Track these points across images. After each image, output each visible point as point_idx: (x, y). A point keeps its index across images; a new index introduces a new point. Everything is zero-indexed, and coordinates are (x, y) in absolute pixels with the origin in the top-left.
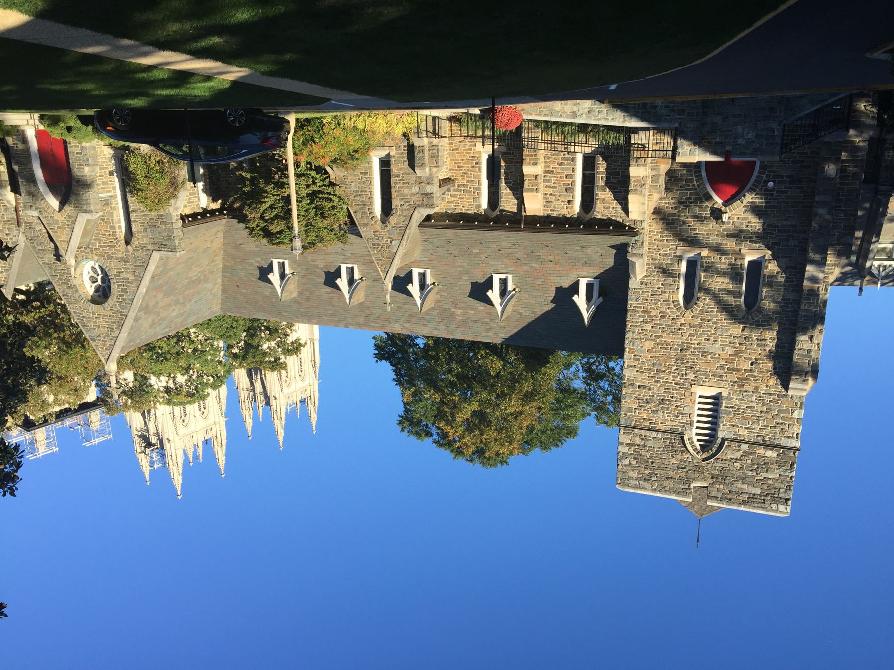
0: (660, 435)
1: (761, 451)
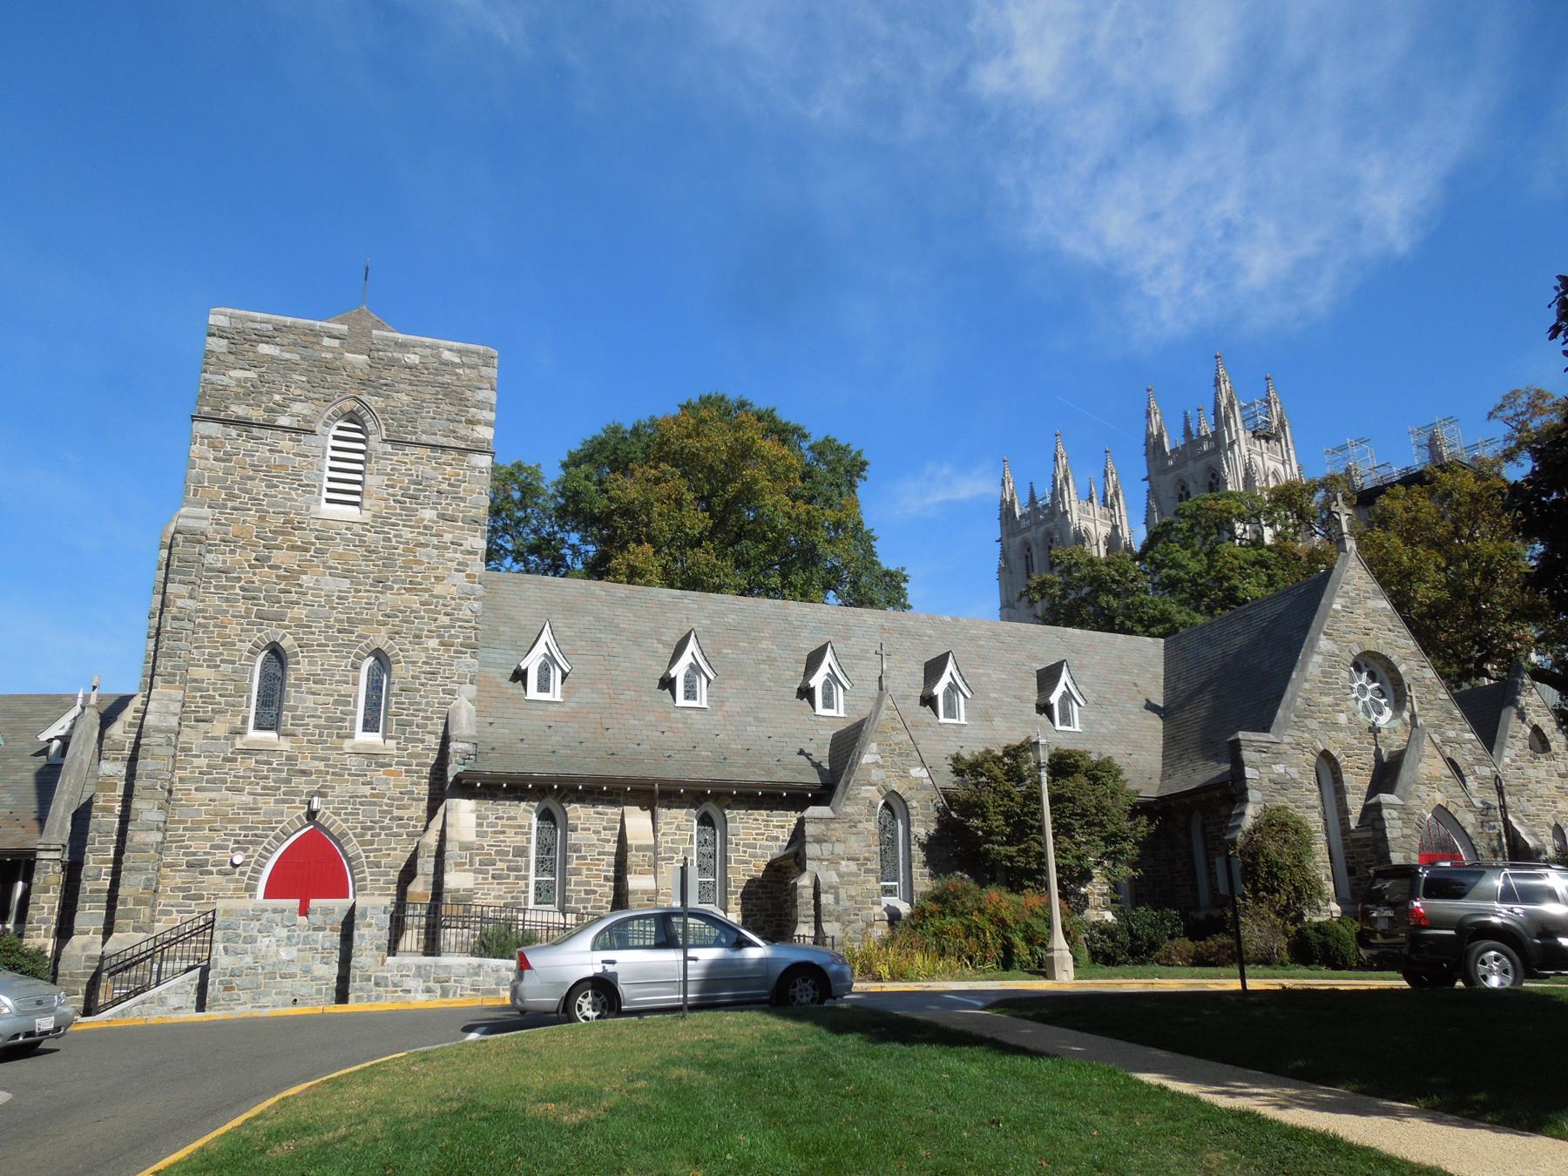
0: (424, 438)
1: (257, 415)
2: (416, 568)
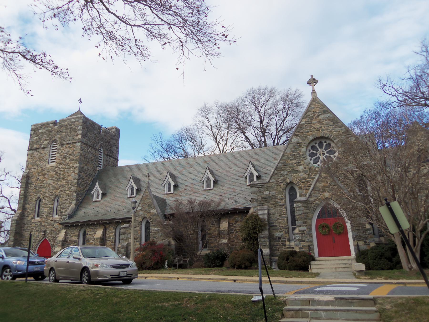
0: (68, 142)
2: (65, 174)
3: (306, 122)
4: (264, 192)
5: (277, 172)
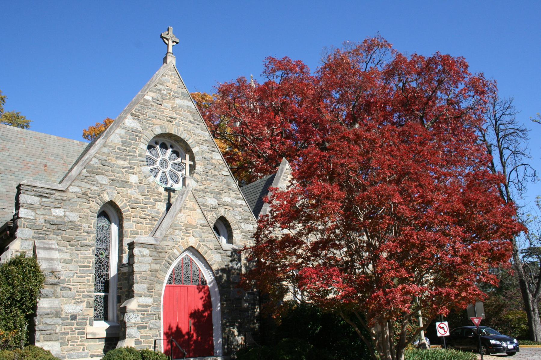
3: (153, 98)
4: (53, 210)
5: (87, 174)
